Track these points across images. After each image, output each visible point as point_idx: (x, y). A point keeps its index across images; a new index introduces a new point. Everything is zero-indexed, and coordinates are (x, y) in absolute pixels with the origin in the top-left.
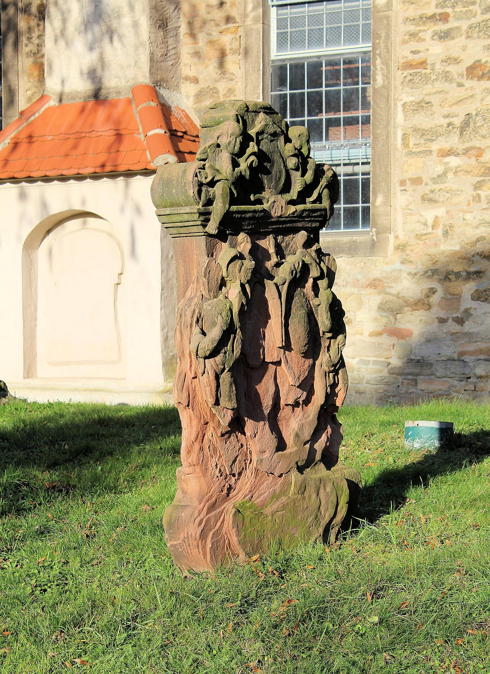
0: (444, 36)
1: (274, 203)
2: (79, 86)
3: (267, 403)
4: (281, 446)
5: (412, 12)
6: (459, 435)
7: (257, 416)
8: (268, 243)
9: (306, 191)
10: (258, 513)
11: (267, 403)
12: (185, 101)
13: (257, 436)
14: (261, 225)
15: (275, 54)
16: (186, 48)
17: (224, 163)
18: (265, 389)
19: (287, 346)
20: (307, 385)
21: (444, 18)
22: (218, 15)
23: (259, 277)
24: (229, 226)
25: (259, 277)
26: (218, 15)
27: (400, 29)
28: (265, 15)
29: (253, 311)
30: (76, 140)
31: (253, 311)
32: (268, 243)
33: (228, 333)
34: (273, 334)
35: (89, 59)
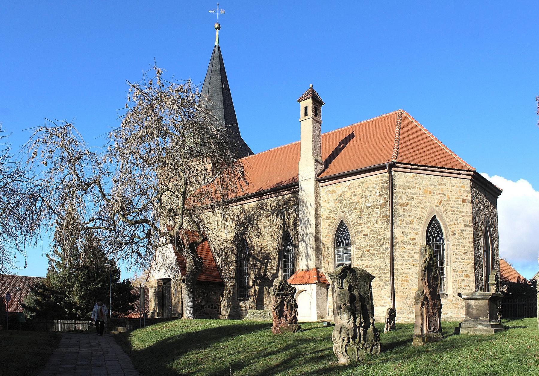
0: (362, 260)
1: (285, 292)
2: (305, 268)
3: (285, 315)
4: (287, 320)
5: (357, 256)
6: (127, 284)
7: (283, 317)
8: (285, 297)
9: (290, 291)
10: (283, 328)
11: (285, 315)
12: (322, 271)
13: (283, 320)
14: (283, 295)
15: (337, 263)
16: (323, 262)
17: (277, 287)
18: (284, 314)
19: (287, 309)
20: (291, 314)
21: (362, 257)
22: (328, 256)
23: (283, 300)
24: (278, 295)
25: (283, 300)
26: (328, 256)
27: (355, 259)
28: (335, 256)
29: (282, 305)
30: (303, 277)
31: (282, 305)
32: (285, 297)
33: (278, 307)
34: (285, 307)
35: (306, 263)
